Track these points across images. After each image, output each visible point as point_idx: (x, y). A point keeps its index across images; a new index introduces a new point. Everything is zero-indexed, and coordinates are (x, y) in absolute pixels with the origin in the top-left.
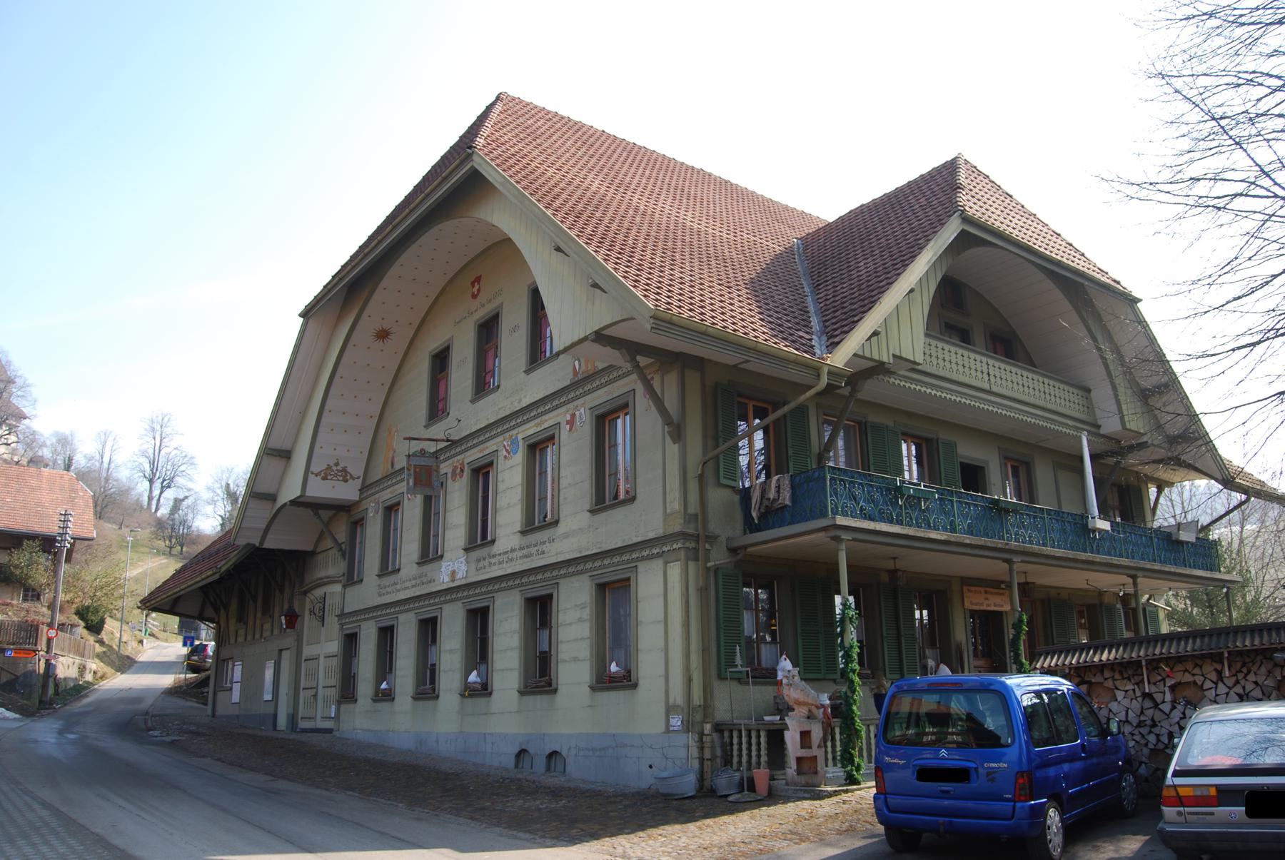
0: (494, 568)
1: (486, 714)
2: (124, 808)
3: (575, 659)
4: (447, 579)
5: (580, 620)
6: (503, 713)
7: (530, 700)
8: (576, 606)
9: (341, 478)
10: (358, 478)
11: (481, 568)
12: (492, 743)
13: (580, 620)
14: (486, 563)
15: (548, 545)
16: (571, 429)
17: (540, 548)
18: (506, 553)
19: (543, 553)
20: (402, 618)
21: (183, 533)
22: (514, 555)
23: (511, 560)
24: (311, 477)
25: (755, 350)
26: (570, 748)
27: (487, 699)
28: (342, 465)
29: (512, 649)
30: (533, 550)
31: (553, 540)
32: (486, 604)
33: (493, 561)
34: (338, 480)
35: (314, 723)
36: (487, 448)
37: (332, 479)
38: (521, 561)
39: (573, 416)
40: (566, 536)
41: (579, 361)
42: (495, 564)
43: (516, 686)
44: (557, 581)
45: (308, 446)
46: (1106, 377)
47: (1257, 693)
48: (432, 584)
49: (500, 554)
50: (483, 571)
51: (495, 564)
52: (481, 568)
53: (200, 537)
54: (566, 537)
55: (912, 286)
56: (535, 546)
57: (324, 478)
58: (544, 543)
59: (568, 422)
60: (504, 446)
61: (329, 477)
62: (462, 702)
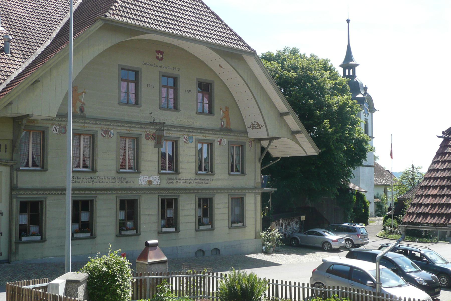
2: (37, 82)
9: (258, 127)
10: (264, 126)
16: (220, 144)
17: (208, 181)
26: (222, 247)
31: (212, 180)
34: (258, 128)
36: (172, 134)
37: (255, 129)
38: (196, 184)
39: (221, 140)
41: (223, 122)
43: (194, 228)
46: (170, 99)
47: (74, 18)
57: (253, 129)
58: (208, 180)
60: (184, 137)
61: (254, 128)
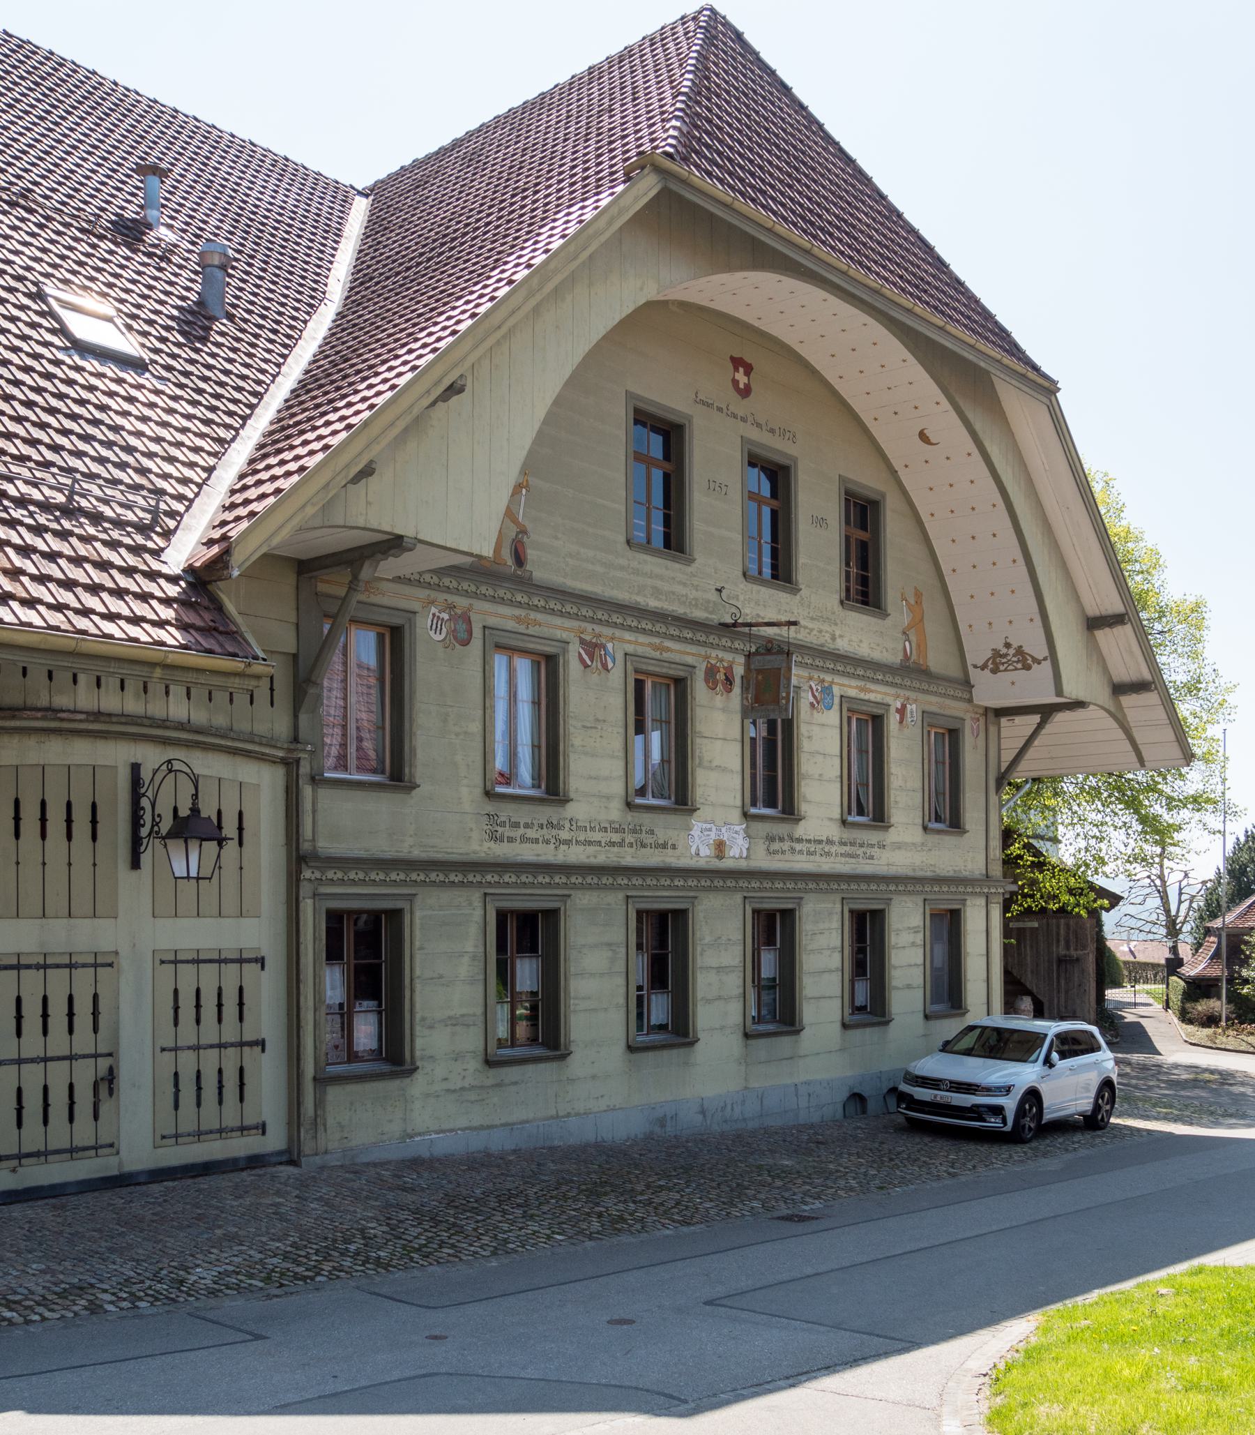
0: (798, 857)
1: (791, 1058)
3: (909, 987)
4: (705, 851)
5: (913, 944)
6: (818, 1054)
7: (856, 1034)
8: (909, 928)
11: (776, 852)
12: (809, 1095)
13: (913, 944)
14: (786, 846)
15: (876, 849)
18: (820, 842)
19: (872, 858)
20: (583, 899)
21: (183, 627)
22: (833, 849)
23: (828, 854)
24: (1046, 653)
25: (645, 610)
27: (794, 1038)
28: (1015, 645)
29: (830, 971)
30: (860, 851)
32: (790, 906)
33: (798, 847)
35: (113, 1160)
37: (1006, 670)
38: (839, 859)
40: (899, 846)
42: (801, 852)
44: (890, 896)
45: (1004, 479)
48: (670, 851)
49: (809, 841)
50: (777, 857)
51: (801, 852)
52: (776, 852)
53: (1108, 988)
54: (899, 848)
55: (528, 567)
56: (861, 846)
58: (872, 846)
59: (898, 711)
60: (811, 687)
61: (1002, 668)
62: (746, 1046)
